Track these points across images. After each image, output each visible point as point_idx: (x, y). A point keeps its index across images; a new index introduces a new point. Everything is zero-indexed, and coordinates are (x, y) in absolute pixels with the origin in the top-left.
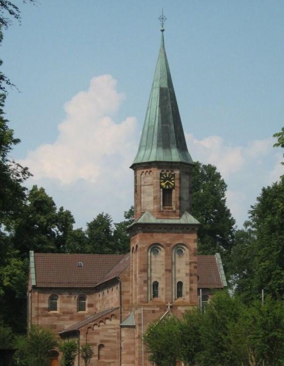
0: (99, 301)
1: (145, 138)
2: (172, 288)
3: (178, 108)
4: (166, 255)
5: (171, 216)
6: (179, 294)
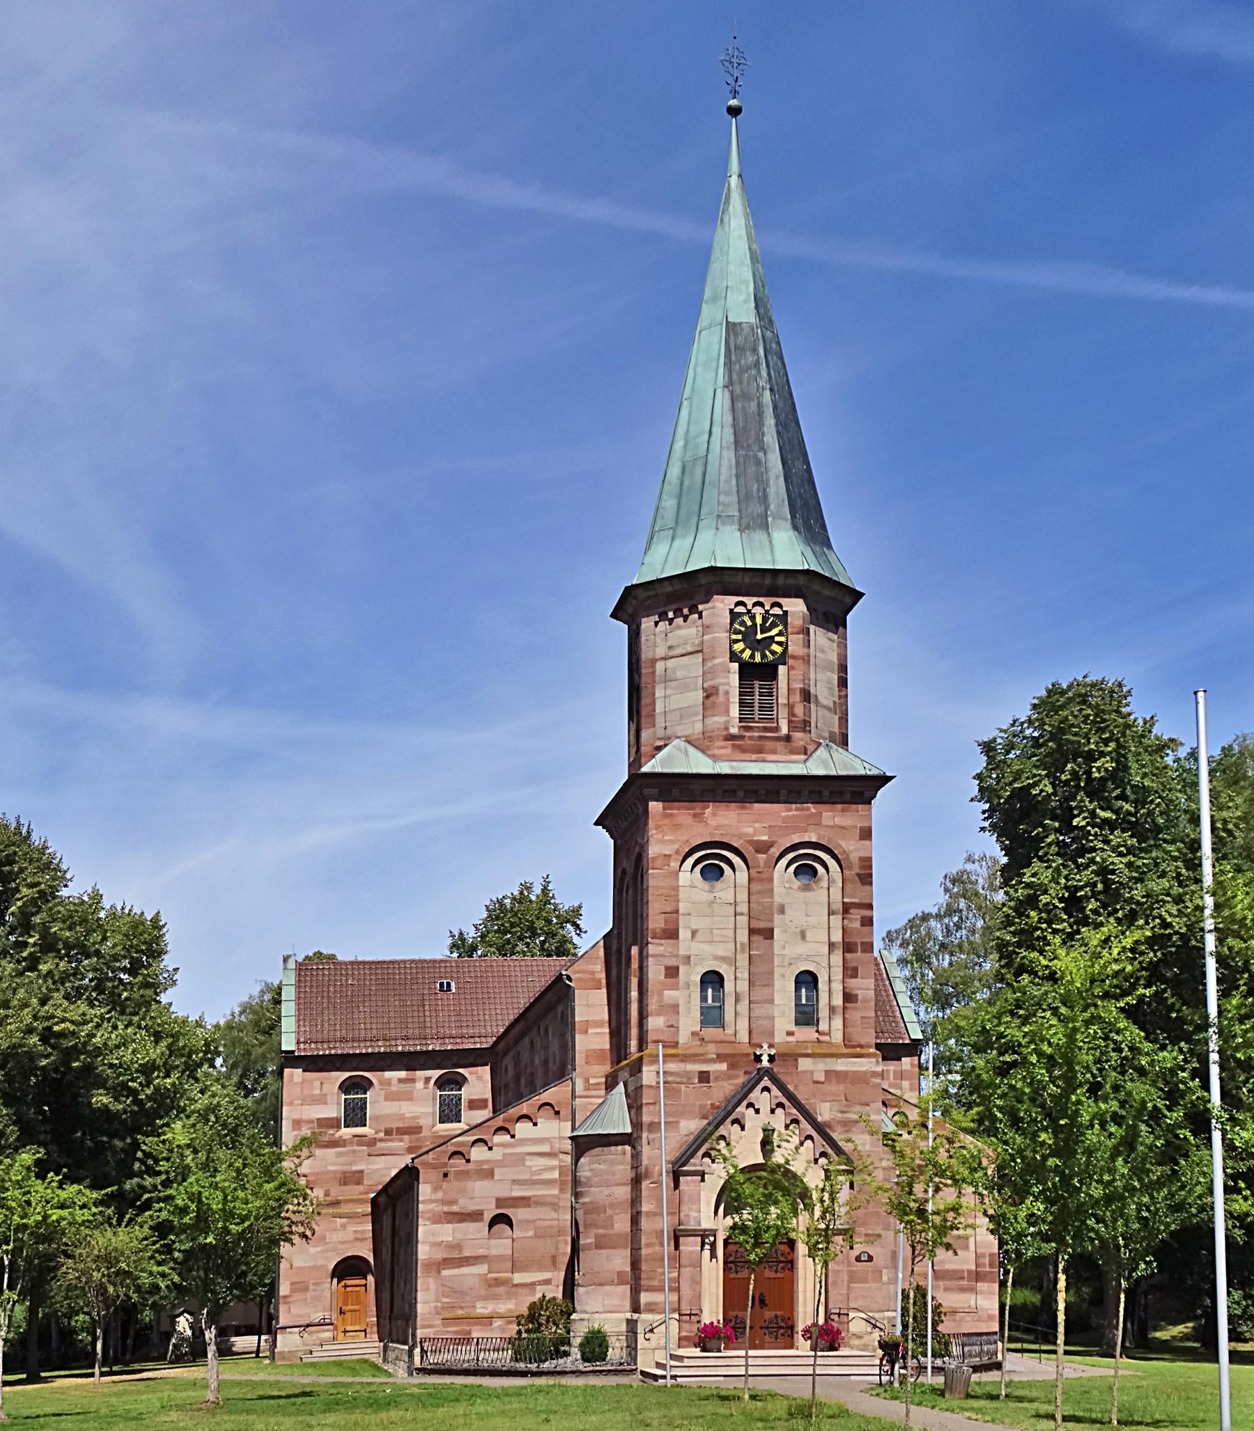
5: (774, 752)
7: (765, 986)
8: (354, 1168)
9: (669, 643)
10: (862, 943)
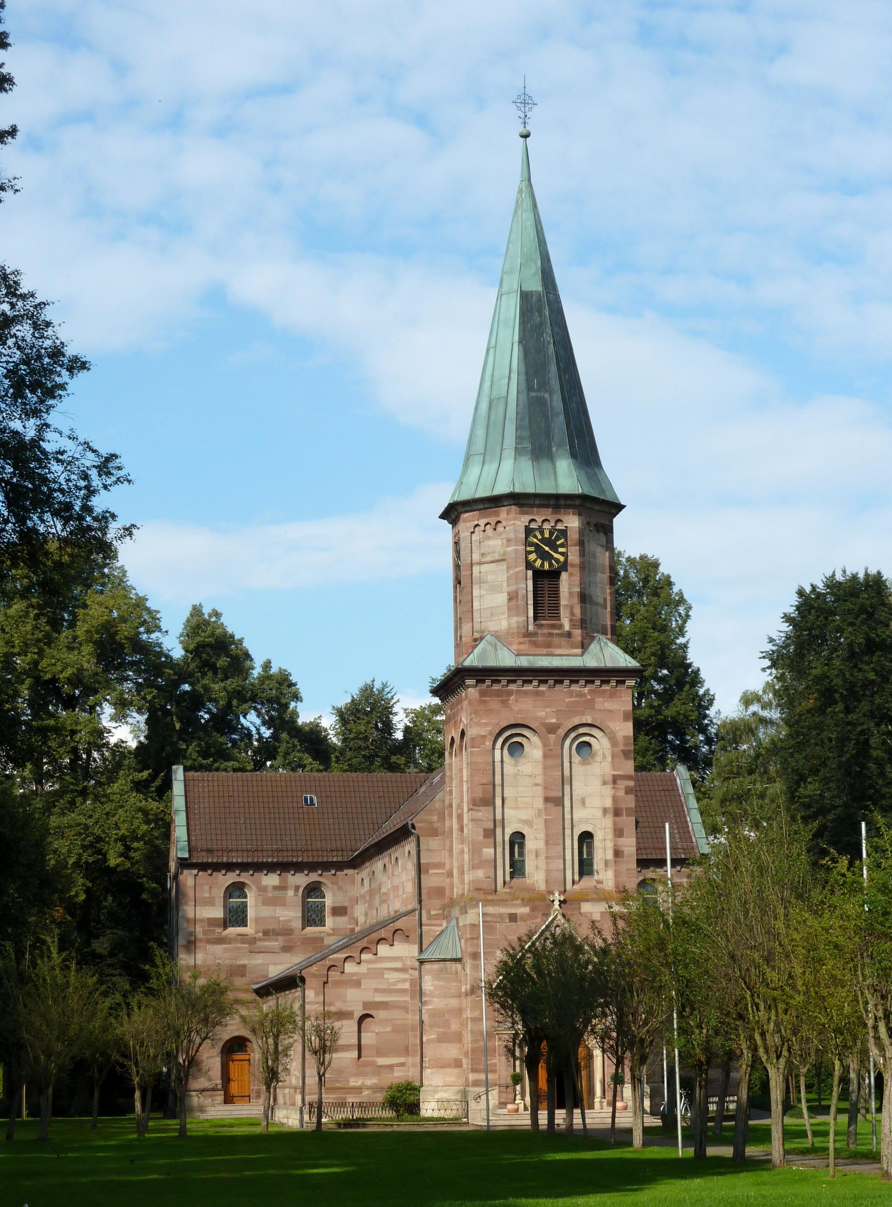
0: (363, 897)
1: (481, 432)
2: (564, 849)
3: (571, 349)
4: (545, 756)
5: (559, 646)
6: (585, 867)
7: (556, 844)
8: (239, 962)
9: (482, 551)
10: (626, 809)
